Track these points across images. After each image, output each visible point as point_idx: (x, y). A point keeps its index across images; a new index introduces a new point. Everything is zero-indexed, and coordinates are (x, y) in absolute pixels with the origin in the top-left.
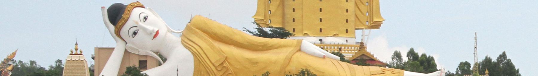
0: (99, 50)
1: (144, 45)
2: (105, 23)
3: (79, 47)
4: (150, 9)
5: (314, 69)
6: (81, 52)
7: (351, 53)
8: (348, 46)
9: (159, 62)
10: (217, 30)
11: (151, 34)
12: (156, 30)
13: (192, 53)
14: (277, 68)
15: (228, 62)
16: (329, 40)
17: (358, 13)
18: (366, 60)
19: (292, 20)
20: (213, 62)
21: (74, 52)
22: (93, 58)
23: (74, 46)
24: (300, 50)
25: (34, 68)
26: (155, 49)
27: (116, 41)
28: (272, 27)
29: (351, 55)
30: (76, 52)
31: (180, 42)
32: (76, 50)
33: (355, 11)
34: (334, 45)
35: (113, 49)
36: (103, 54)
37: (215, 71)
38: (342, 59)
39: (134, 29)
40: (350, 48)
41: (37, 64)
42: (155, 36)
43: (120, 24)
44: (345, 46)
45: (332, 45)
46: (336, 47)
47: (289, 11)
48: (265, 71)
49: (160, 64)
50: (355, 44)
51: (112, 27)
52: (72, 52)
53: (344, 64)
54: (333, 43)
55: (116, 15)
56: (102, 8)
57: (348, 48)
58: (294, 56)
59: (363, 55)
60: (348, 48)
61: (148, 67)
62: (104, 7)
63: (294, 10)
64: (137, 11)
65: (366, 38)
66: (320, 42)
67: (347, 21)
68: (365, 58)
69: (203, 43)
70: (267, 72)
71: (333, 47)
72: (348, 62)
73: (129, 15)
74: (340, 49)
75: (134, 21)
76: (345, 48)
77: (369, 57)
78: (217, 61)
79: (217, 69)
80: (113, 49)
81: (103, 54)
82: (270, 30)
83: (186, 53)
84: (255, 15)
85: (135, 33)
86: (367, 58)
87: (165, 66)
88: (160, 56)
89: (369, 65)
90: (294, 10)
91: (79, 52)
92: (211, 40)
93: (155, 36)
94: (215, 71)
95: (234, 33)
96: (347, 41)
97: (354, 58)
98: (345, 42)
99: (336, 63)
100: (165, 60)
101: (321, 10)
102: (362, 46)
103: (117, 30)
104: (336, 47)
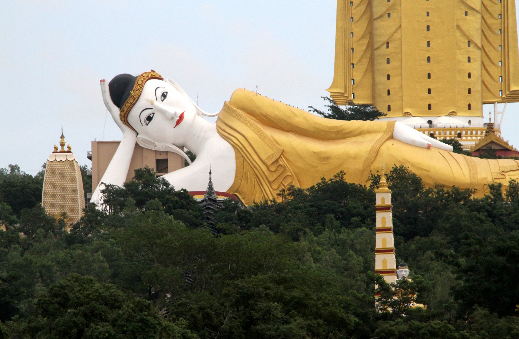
0: (98, 145)
1: (162, 136)
2: (106, 104)
3: (66, 141)
5: (413, 165)
6: (69, 148)
7: (472, 140)
8: (472, 130)
9: (186, 160)
10: (269, 111)
11: (172, 118)
12: (179, 114)
13: (235, 146)
14: (359, 165)
15: (285, 158)
16: (443, 121)
17: (487, 78)
18: (495, 151)
19: (387, 93)
20: (264, 158)
22: (90, 158)
23: (59, 140)
24: (392, 137)
25: (17, 176)
26: (180, 142)
27: (123, 131)
29: (473, 143)
30: (63, 149)
31: (216, 131)
32: (62, 145)
33: (482, 76)
34: (451, 129)
35: (118, 143)
36: (103, 150)
37: (267, 173)
38: (458, 149)
39: (147, 113)
40: (474, 132)
41: (21, 170)
42: (178, 122)
43: (128, 105)
44: (467, 130)
45: (448, 130)
46: (453, 133)
47: (381, 79)
48: (338, 171)
49: (186, 164)
50: (482, 126)
51: (116, 110)
52: (56, 148)
53: (460, 157)
54: (448, 126)
55: (122, 91)
56: (101, 81)
57: (472, 133)
58: (384, 147)
59: (492, 142)
60: (472, 133)
61: (169, 171)
62: (104, 81)
63: (389, 77)
65: (499, 116)
66: (428, 125)
67: (470, 91)
68: (494, 147)
69: (248, 130)
71: (448, 132)
72: (468, 154)
73: (141, 91)
74: (459, 135)
75: (148, 100)
76: (466, 134)
77: (500, 146)
78: (269, 157)
79: (269, 170)
80: (118, 143)
81: (103, 150)
82: (350, 109)
83: (225, 146)
84: (331, 87)
85: (149, 119)
86: (497, 148)
87: (194, 167)
89: (500, 158)
90: (389, 77)
94: (267, 173)
95: (294, 113)
96: (470, 122)
97: (477, 148)
98: (467, 125)
99: (446, 154)
100: (193, 158)
101: (429, 76)
102: (490, 128)
103: (123, 114)
104: (453, 133)
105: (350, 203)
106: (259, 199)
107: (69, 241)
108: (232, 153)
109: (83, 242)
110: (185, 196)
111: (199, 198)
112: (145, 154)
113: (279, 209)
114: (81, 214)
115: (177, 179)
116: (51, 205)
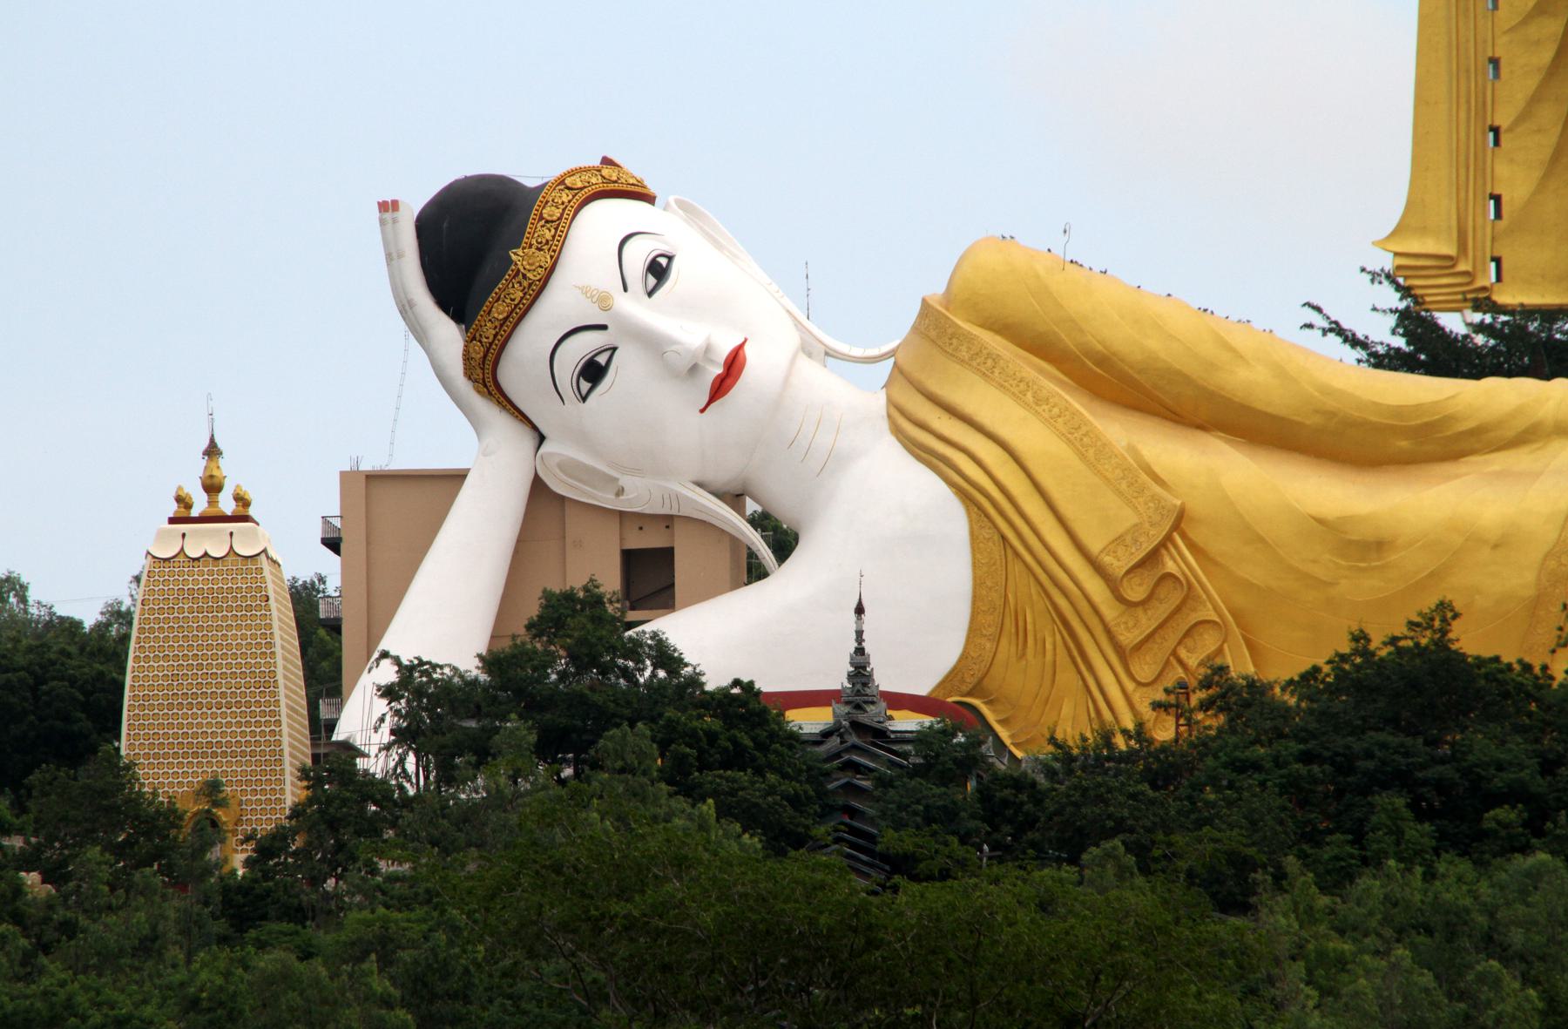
0: (371, 488)
1: (643, 444)
2: (406, 309)
3: (232, 472)
4: (682, 205)
6: (242, 500)
9: (752, 555)
12: (724, 349)
13: (967, 494)
15: (1192, 546)
20: (1095, 546)
21: (200, 505)
22: (333, 544)
23: (199, 465)
26: (725, 472)
28: (1496, 309)
30: (213, 503)
32: (212, 487)
37: (1110, 611)
39: (586, 344)
41: (32, 596)
42: (720, 388)
48: (1429, 602)
49: (756, 572)
51: (448, 335)
52: (183, 501)
56: (383, 206)
62: (395, 205)
64: (599, 225)
69: (1028, 422)
70: (1443, 606)
73: (555, 250)
75: (585, 291)
78: (1119, 540)
79: (1120, 598)
81: (392, 511)
82: (1480, 328)
83: (925, 490)
84: (1399, 231)
85: (593, 372)
87: (788, 585)
88: (761, 521)
91: (227, 505)
92: (1077, 404)
93: (720, 388)
94: (1110, 611)
95: (1238, 339)
100: (784, 544)
103: (478, 350)
105: (1480, 742)
106: (1073, 727)
107: (245, 908)
108: (954, 521)
109: (299, 914)
110: (746, 708)
111: (809, 721)
112: (576, 525)
113: (1162, 768)
114: (292, 792)
115: (715, 637)
116: (158, 750)
